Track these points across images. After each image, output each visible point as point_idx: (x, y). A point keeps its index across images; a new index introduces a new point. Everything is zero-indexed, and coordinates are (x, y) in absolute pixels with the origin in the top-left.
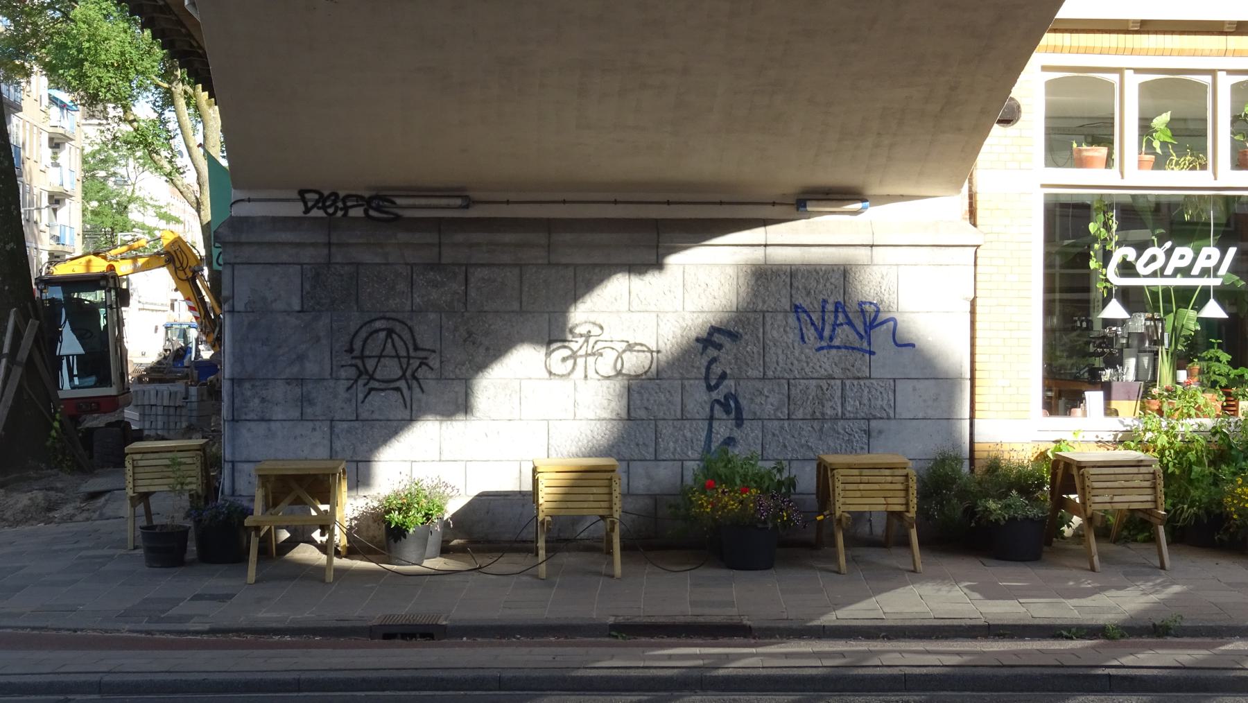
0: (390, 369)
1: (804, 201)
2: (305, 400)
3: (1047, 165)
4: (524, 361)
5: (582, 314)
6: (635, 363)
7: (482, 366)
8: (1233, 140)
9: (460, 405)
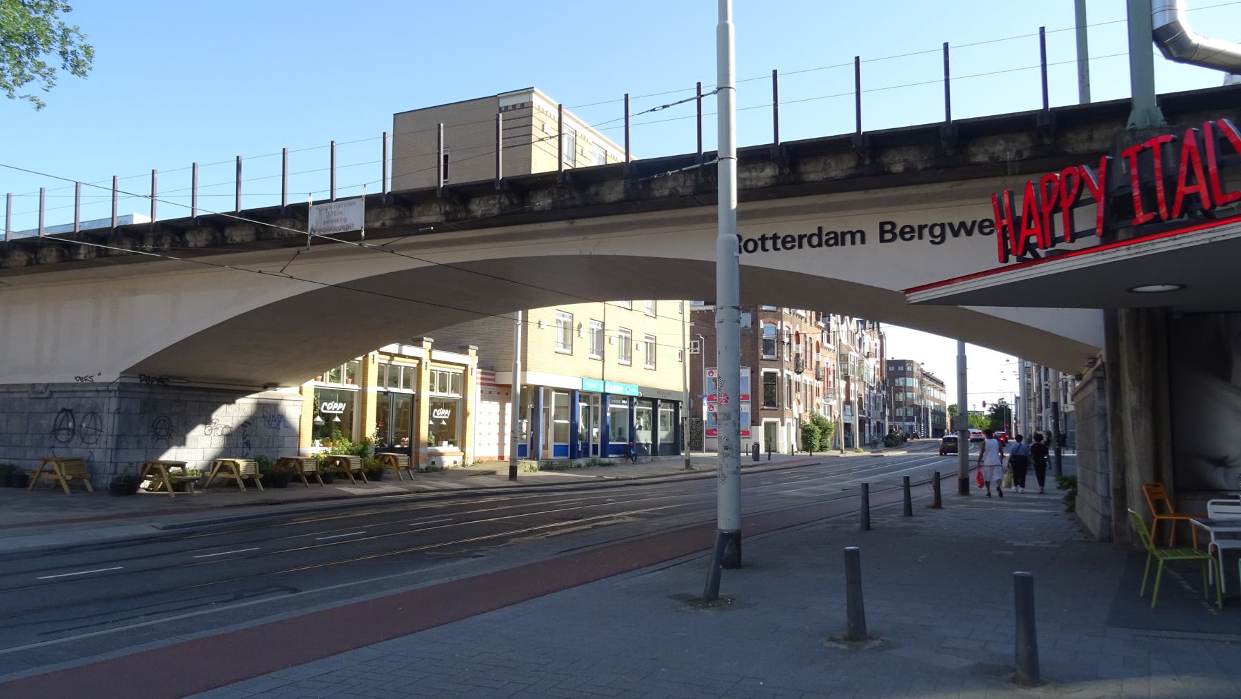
0: (164, 432)
1: (265, 387)
2: (139, 442)
3: (483, 399)
4: (200, 429)
5: (215, 416)
6: (226, 431)
7: (188, 431)
8: (53, 268)
9: (182, 443)
